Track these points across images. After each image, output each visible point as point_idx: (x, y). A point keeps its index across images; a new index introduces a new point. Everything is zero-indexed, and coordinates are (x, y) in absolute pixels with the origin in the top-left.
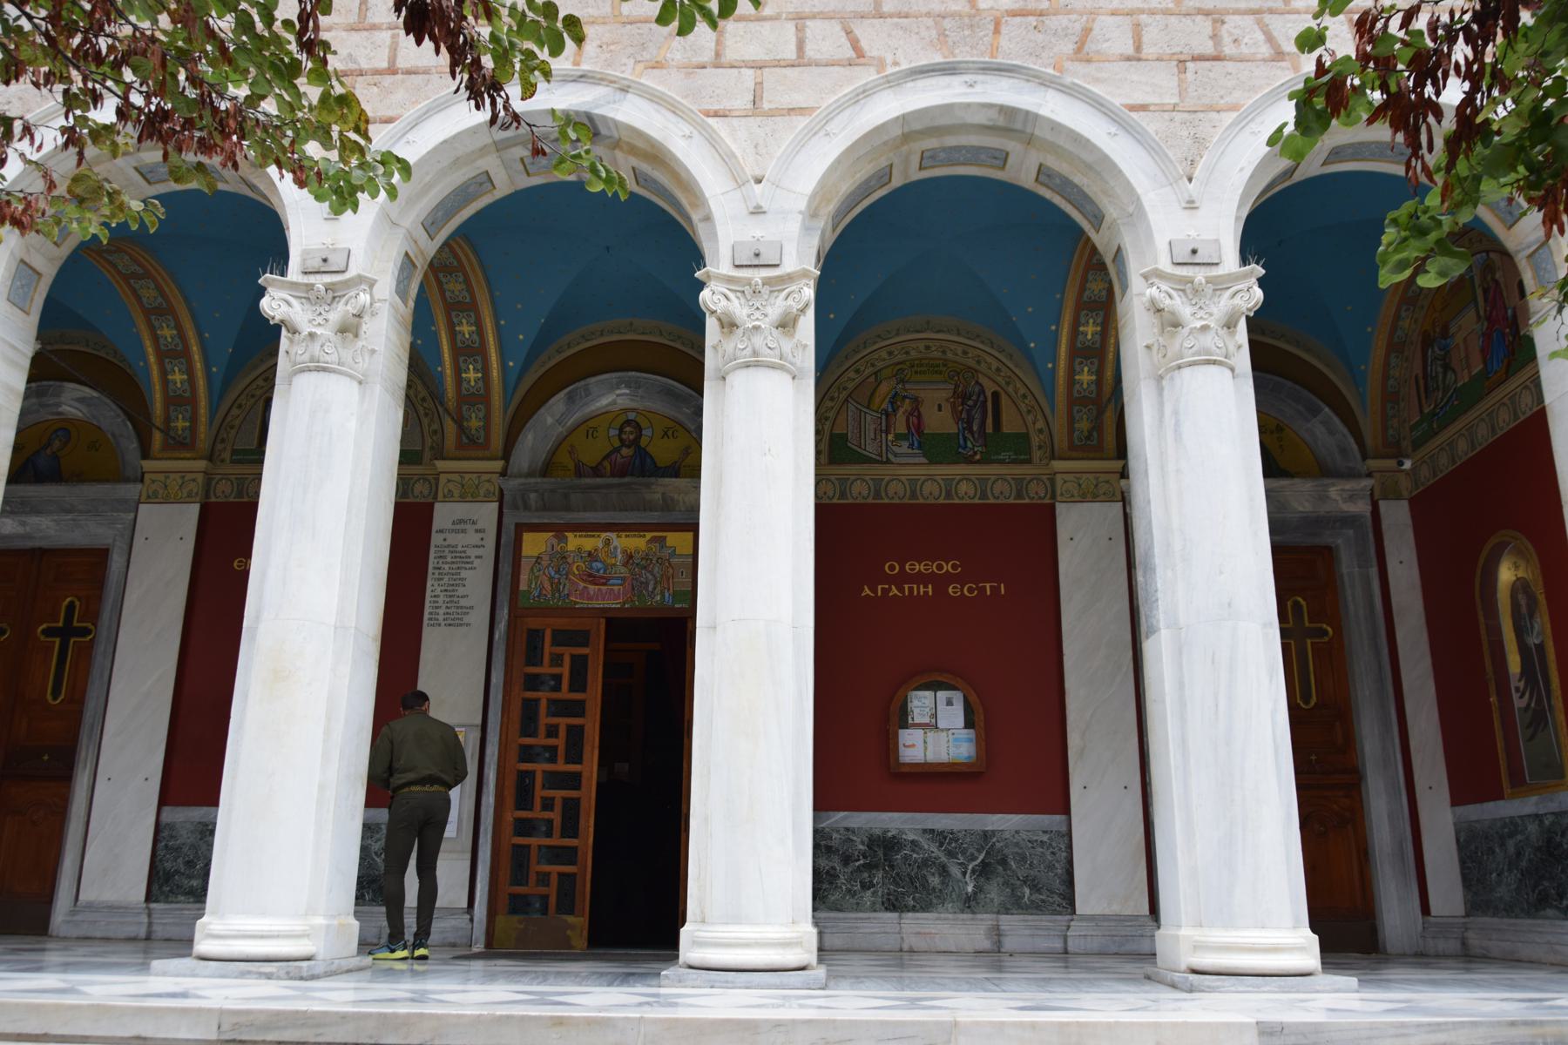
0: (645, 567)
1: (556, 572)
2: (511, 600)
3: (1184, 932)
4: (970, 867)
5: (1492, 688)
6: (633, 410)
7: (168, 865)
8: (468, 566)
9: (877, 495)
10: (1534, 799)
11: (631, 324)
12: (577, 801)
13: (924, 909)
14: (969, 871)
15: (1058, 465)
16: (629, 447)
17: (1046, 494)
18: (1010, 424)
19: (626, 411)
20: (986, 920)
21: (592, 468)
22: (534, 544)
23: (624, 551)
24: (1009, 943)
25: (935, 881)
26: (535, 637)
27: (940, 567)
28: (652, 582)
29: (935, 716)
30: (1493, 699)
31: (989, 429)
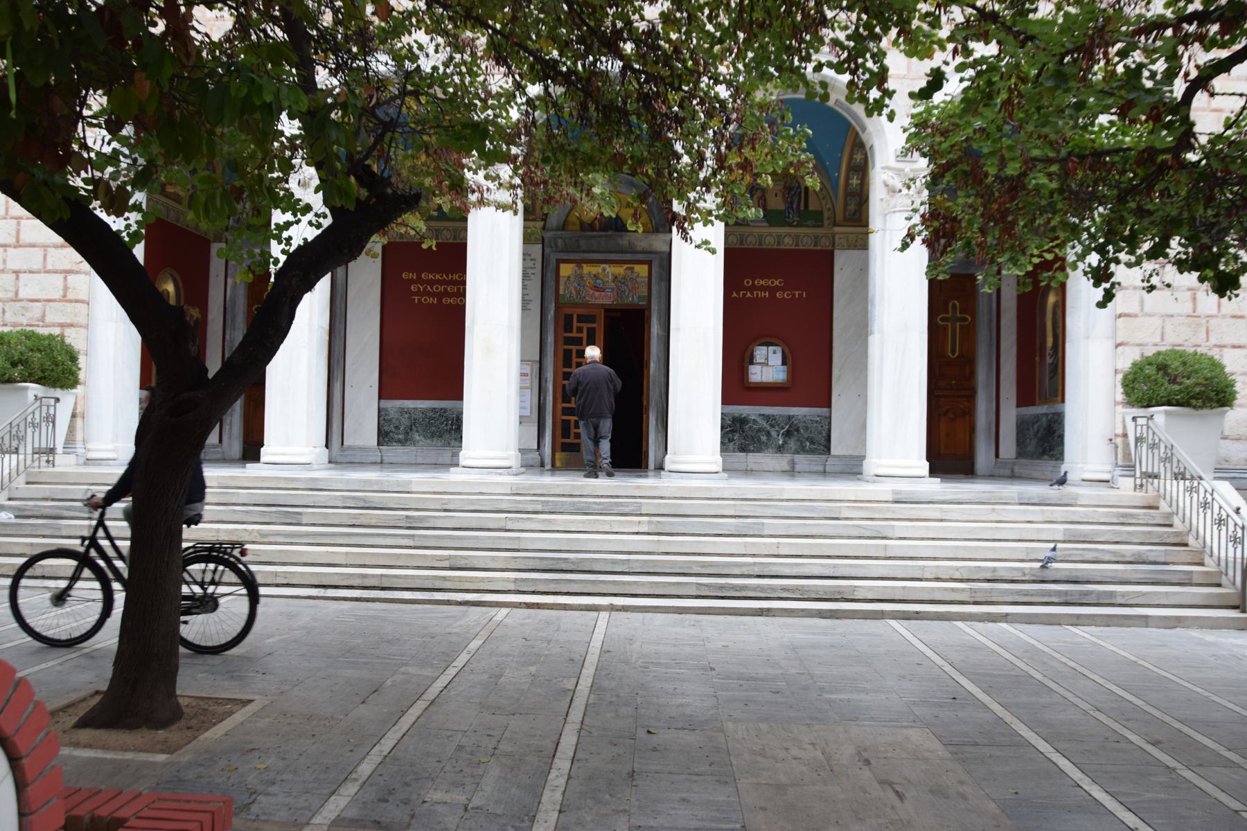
3: (873, 460)
5: (1038, 353)
7: (386, 428)
9: (741, 243)
10: (1046, 406)
13: (758, 452)
15: (837, 229)
18: (813, 206)
20: (788, 457)
22: (566, 270)
23: (613, 274)
24: (798, 468)
25: (764, 438)
26: (568, 319)
27: (773, 283)
29: (767, 359)
30: (1037, 359)
31: (802, 208)
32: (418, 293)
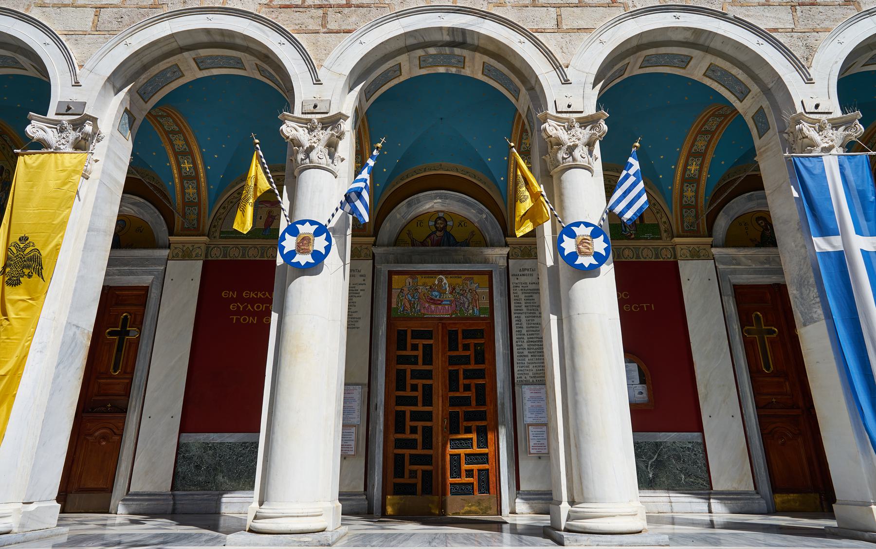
0: (462, 295)
1: (412, 298)
2: (388, 312)
4: (650, 463)
6: (441, 211)
8: (356, 295)
11: (441, 165)
12: (431, 428)
14: (649, 466)
15: (677, 240)
16: (441, 231)
17: (671, 256)
19: (438, 212)
21: (420, 242)
28: (467, 303)
32: (238, 312)
